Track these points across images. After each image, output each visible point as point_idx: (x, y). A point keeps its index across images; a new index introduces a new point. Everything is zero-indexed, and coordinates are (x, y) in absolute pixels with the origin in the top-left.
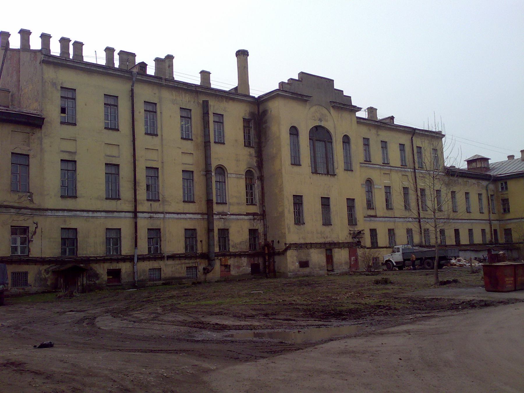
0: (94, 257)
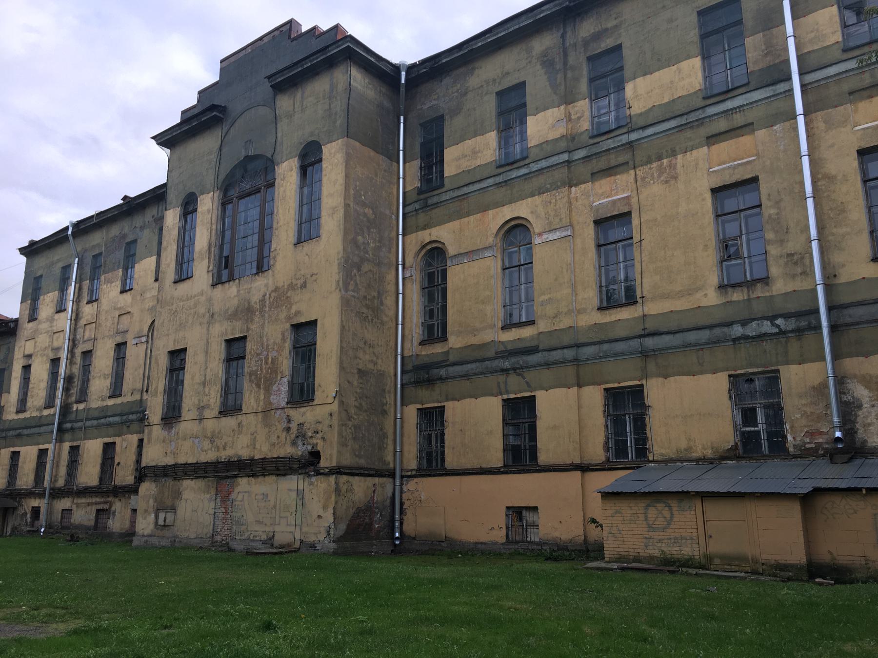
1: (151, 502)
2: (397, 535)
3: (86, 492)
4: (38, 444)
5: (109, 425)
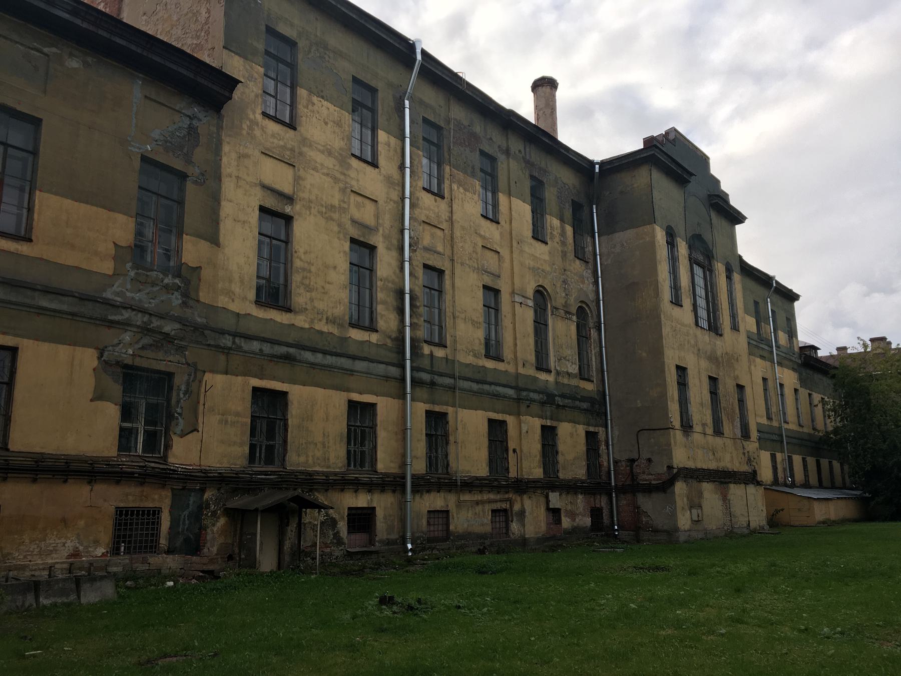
0: (323, 473)
1: (685, 499)
2: (616, 527)
3: (471, 485)
4: (348, 390)
5: (497, 396)
